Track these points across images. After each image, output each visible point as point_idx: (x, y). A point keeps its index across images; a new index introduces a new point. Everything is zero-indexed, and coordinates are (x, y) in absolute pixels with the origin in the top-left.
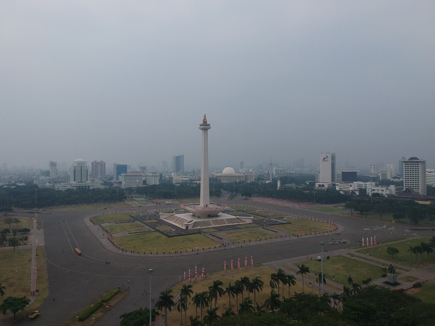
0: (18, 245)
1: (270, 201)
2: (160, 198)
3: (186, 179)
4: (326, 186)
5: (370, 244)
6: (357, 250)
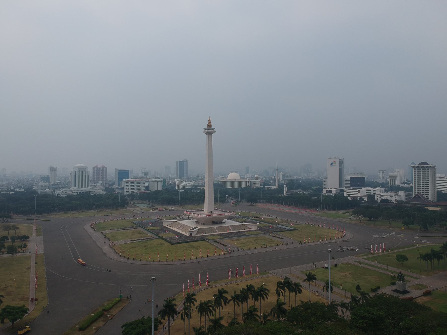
0: (16, 253)
1: (276, 207)
2: (163, 204)
4: (334, 192)
5: (378, 251)
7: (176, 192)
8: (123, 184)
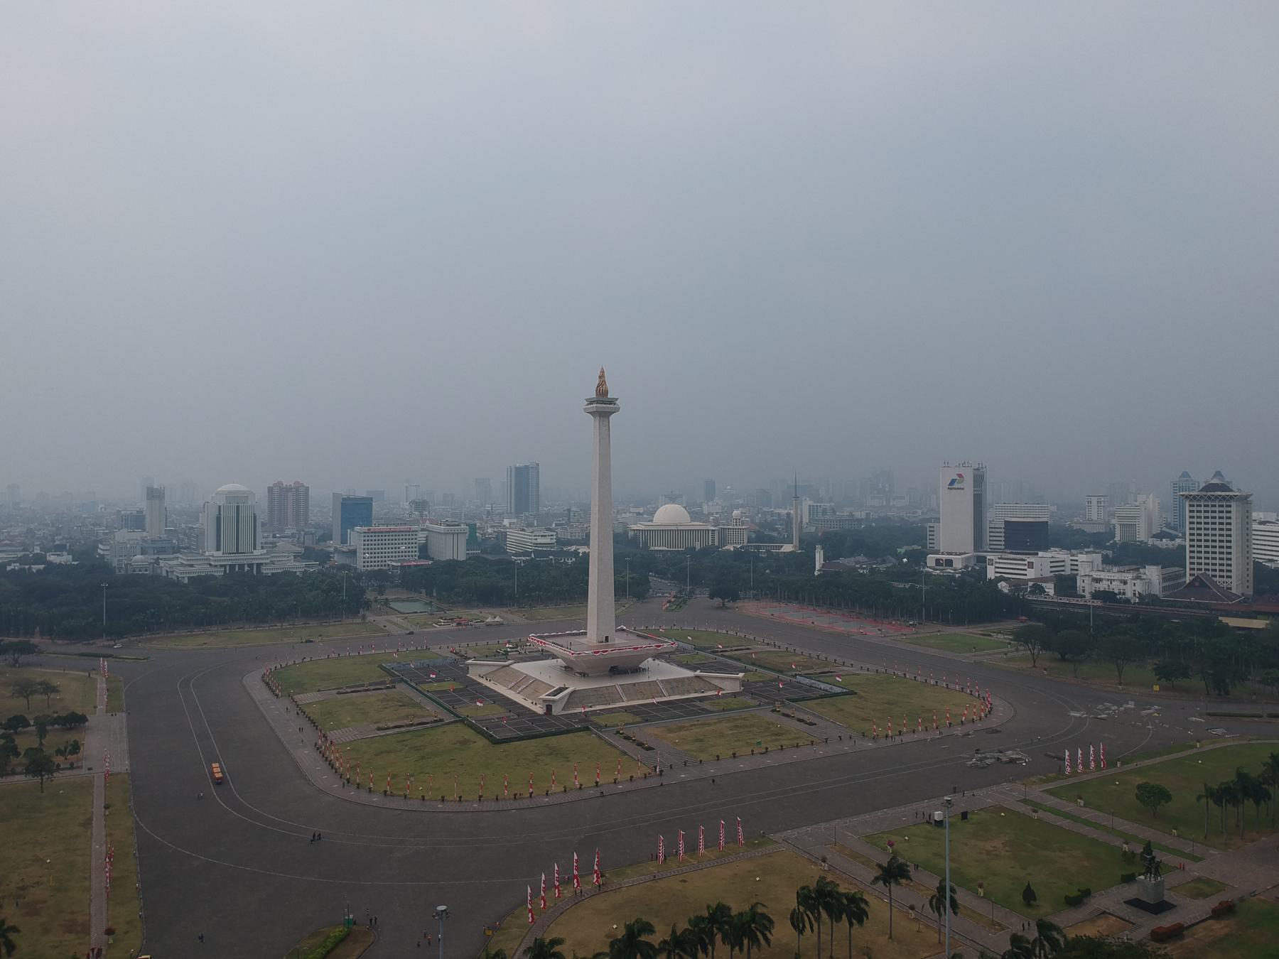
0: (50, 771)
1: (792, 614)
2: (468, 604)
3: (547, 540)
4: (958, 563)
5: (1086, 764)
6: (1050, 786)
7: (506, 567)
8: (356, 538)
